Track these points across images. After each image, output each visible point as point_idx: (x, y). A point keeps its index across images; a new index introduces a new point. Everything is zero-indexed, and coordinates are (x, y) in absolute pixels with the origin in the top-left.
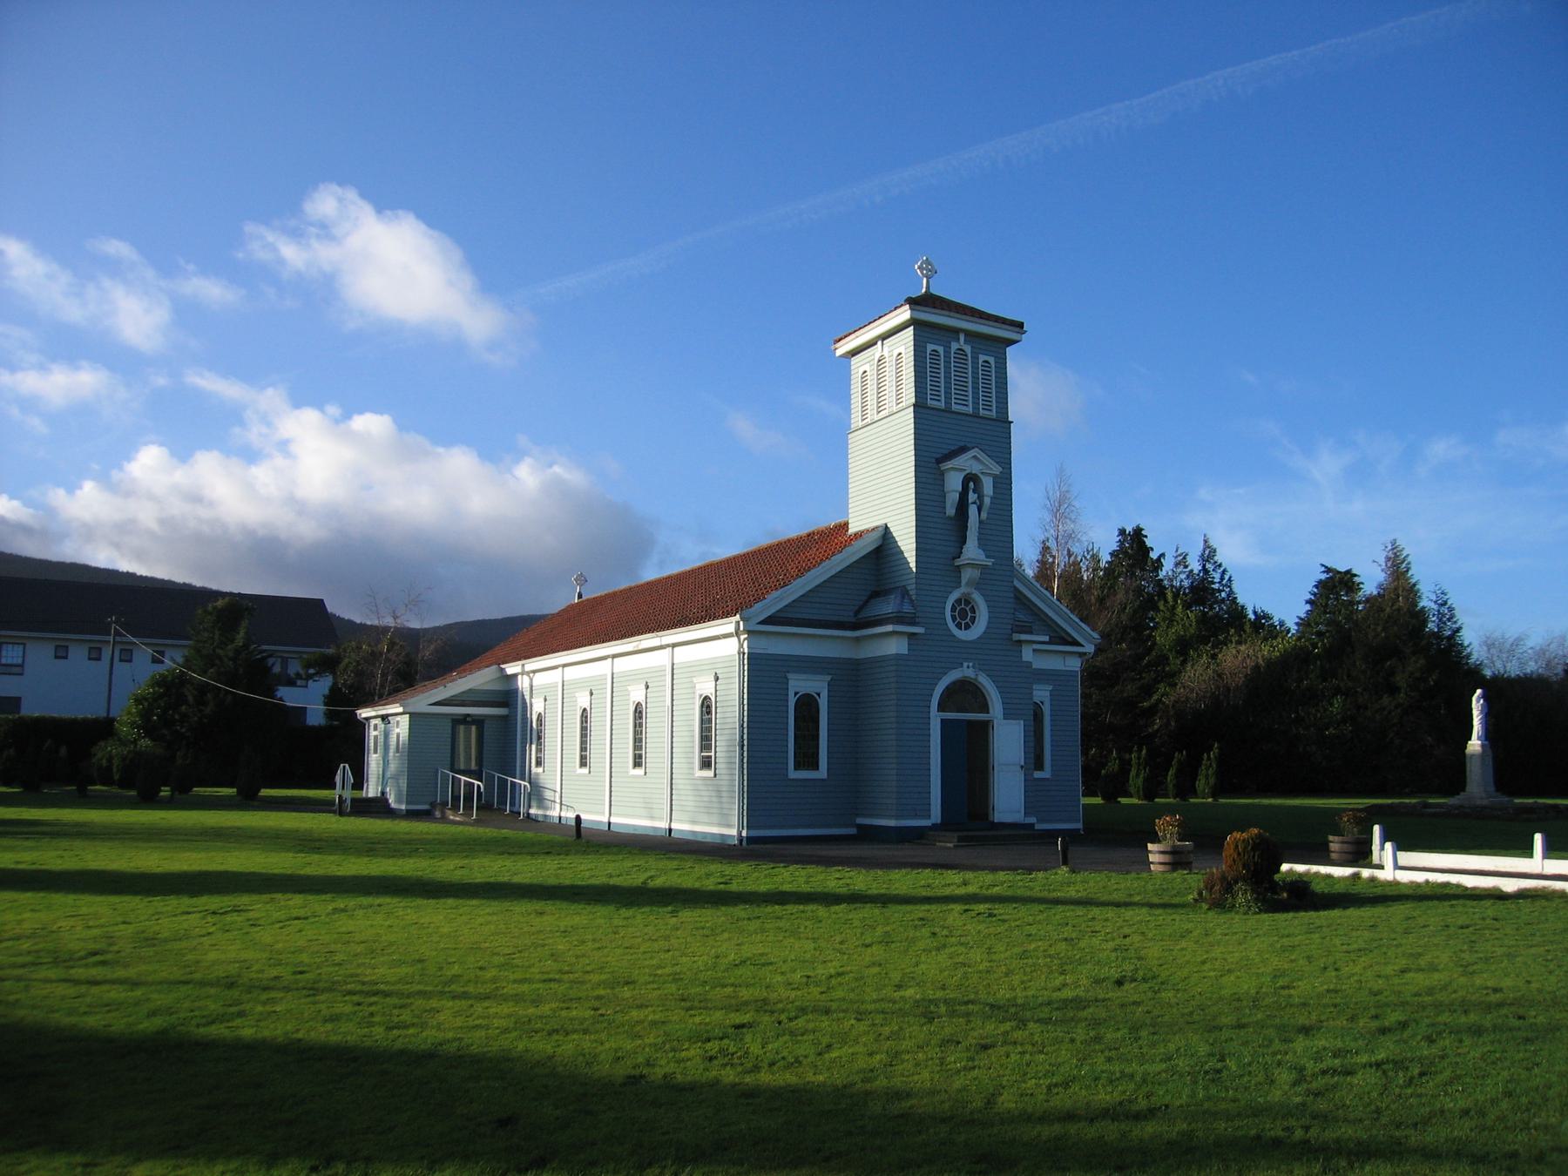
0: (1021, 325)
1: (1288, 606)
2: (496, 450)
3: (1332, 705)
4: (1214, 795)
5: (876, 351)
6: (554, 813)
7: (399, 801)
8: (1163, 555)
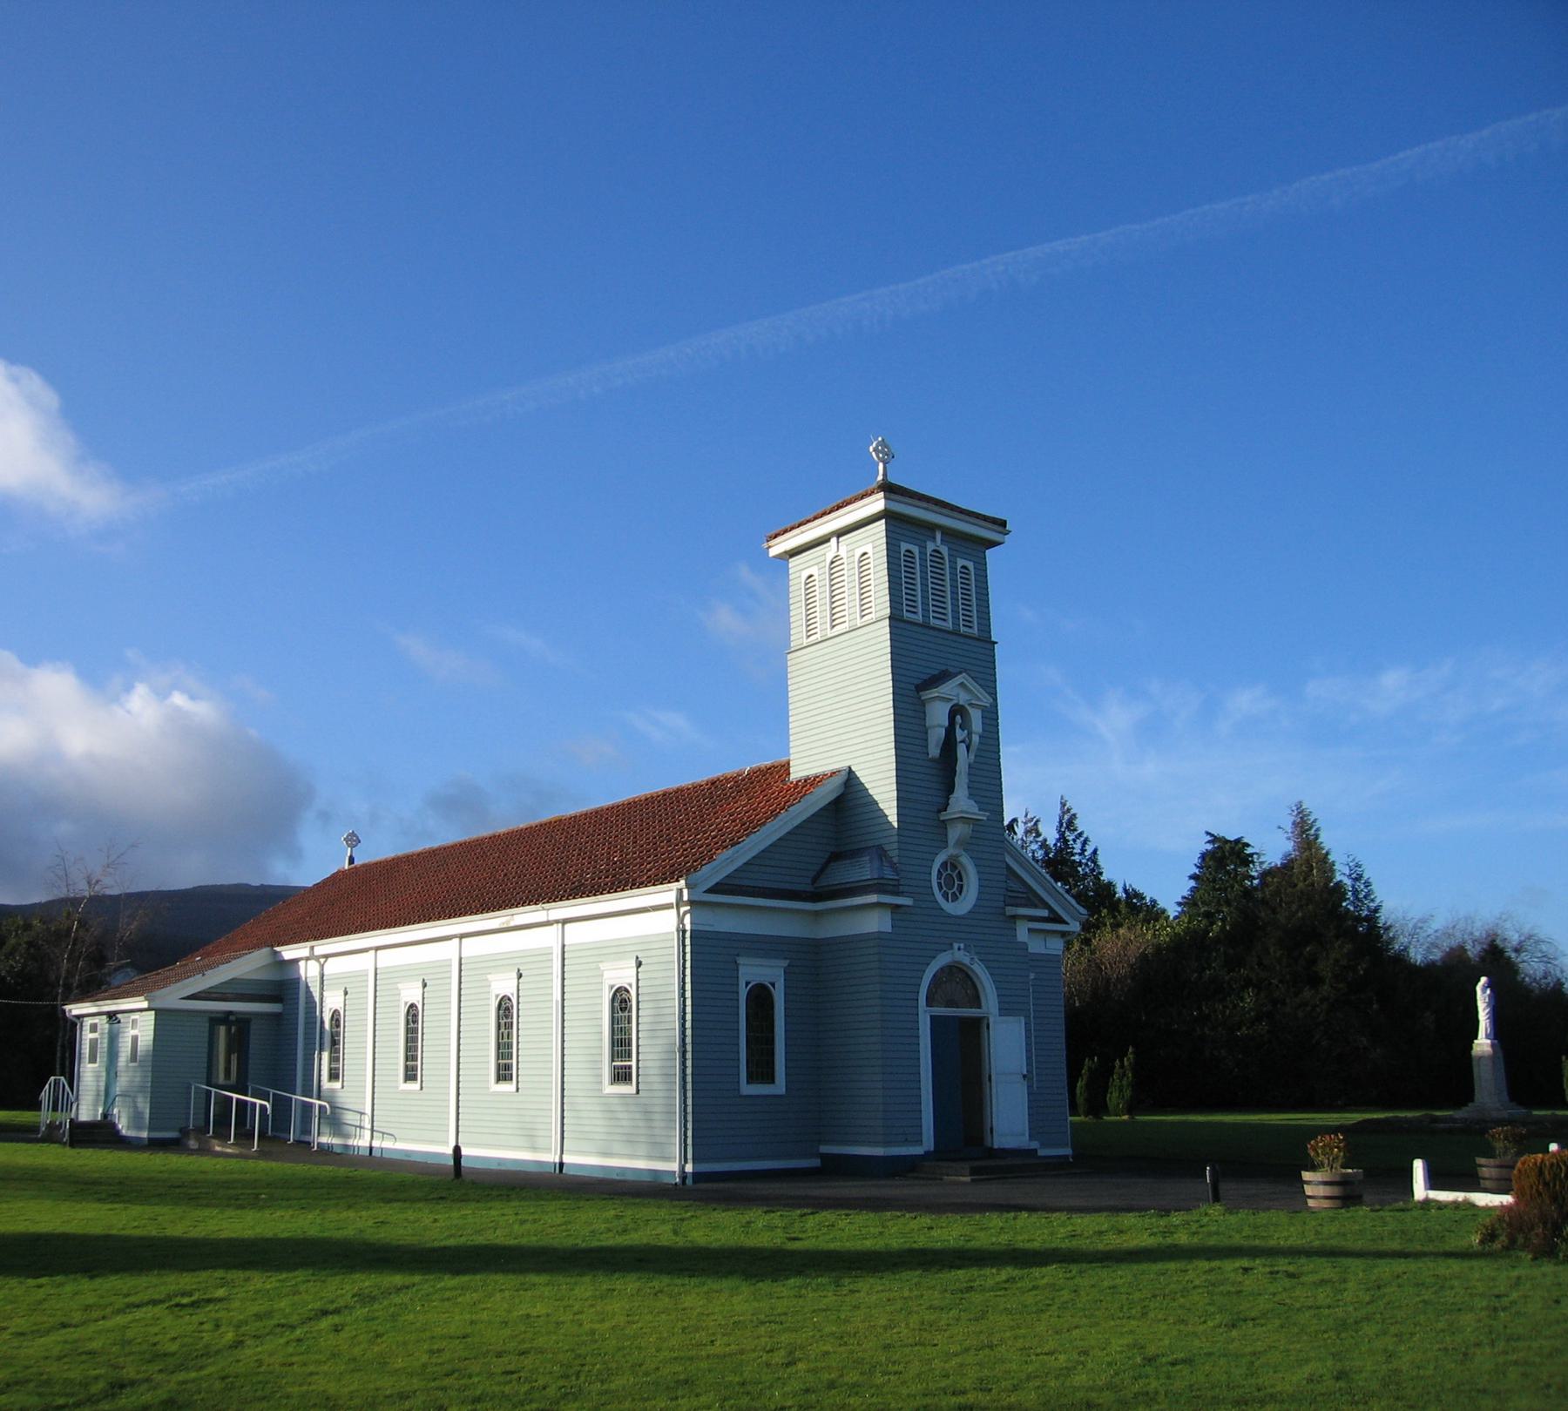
0: (1003, 524)
3: (1242, 999)
4: (1131, 1109)
6: (362, 1141)
7: (136, 1120)
8: (1015, 820)
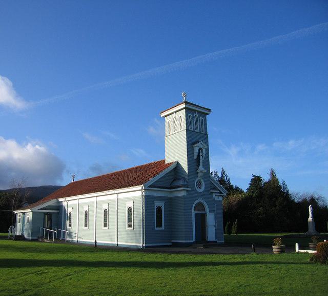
1: (244, 186)
2: (21, 142)
4: (237, 233)
5: (174, 115)
6: (76, 239)
7: (29, 236)
